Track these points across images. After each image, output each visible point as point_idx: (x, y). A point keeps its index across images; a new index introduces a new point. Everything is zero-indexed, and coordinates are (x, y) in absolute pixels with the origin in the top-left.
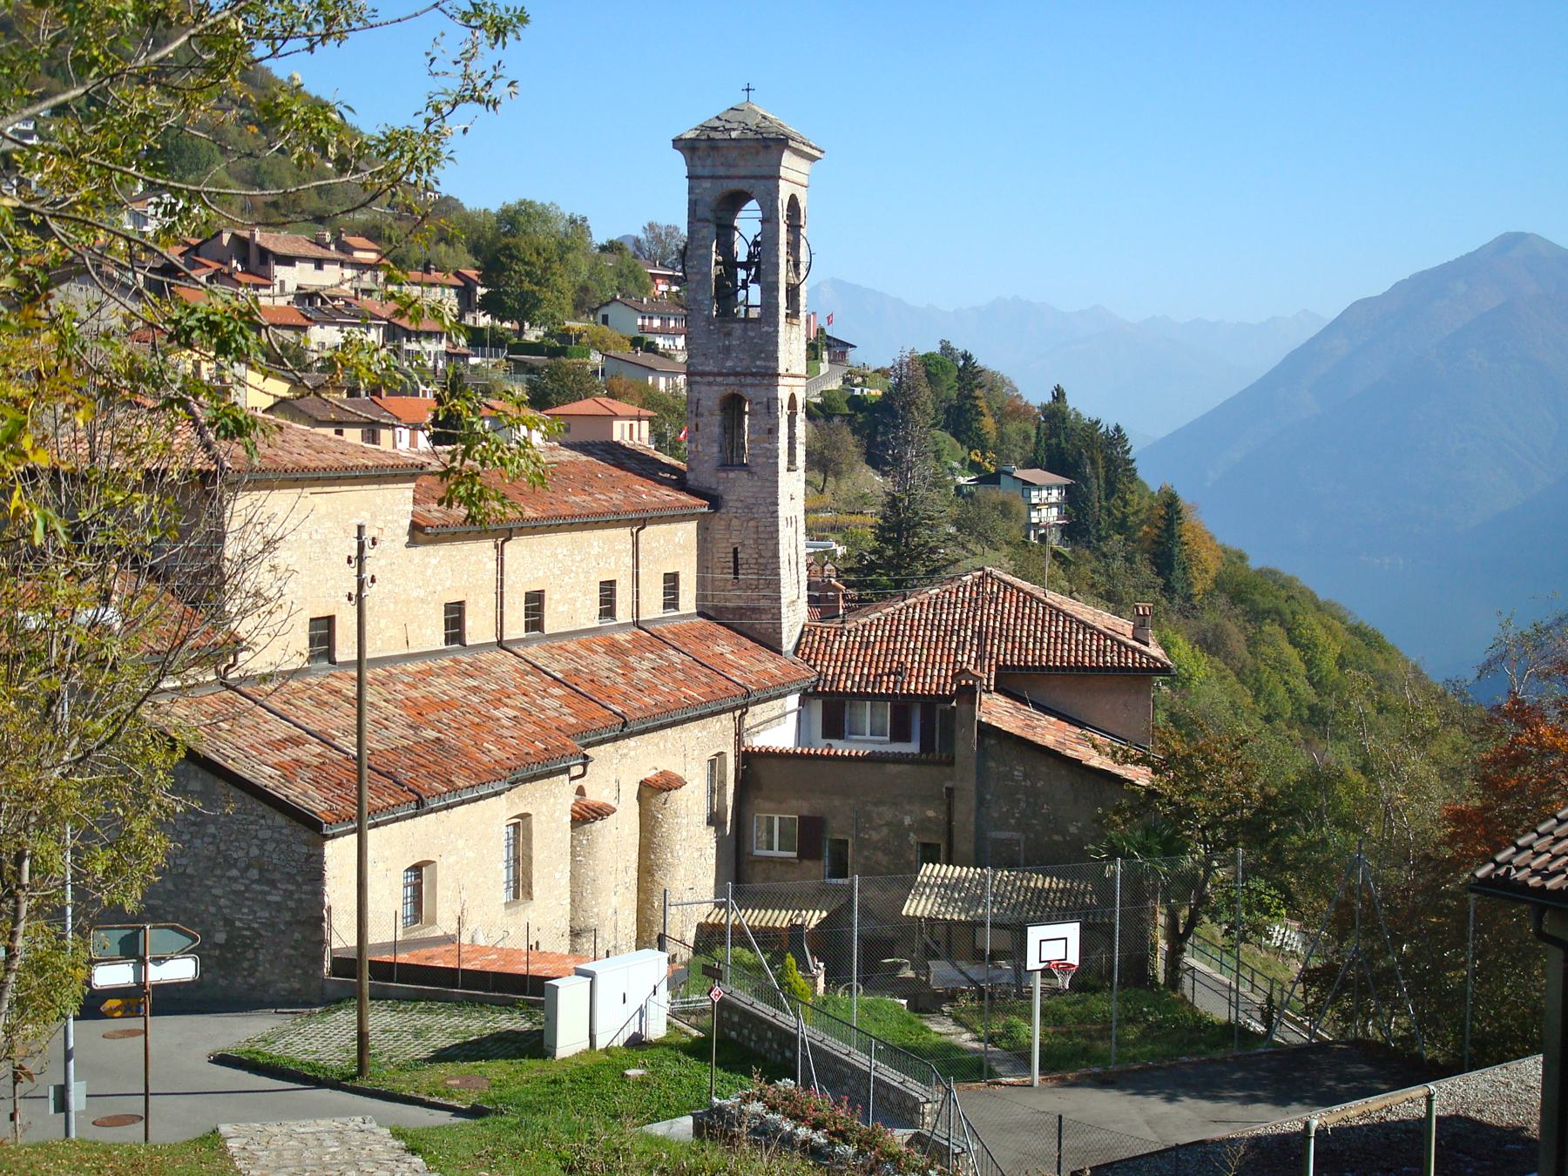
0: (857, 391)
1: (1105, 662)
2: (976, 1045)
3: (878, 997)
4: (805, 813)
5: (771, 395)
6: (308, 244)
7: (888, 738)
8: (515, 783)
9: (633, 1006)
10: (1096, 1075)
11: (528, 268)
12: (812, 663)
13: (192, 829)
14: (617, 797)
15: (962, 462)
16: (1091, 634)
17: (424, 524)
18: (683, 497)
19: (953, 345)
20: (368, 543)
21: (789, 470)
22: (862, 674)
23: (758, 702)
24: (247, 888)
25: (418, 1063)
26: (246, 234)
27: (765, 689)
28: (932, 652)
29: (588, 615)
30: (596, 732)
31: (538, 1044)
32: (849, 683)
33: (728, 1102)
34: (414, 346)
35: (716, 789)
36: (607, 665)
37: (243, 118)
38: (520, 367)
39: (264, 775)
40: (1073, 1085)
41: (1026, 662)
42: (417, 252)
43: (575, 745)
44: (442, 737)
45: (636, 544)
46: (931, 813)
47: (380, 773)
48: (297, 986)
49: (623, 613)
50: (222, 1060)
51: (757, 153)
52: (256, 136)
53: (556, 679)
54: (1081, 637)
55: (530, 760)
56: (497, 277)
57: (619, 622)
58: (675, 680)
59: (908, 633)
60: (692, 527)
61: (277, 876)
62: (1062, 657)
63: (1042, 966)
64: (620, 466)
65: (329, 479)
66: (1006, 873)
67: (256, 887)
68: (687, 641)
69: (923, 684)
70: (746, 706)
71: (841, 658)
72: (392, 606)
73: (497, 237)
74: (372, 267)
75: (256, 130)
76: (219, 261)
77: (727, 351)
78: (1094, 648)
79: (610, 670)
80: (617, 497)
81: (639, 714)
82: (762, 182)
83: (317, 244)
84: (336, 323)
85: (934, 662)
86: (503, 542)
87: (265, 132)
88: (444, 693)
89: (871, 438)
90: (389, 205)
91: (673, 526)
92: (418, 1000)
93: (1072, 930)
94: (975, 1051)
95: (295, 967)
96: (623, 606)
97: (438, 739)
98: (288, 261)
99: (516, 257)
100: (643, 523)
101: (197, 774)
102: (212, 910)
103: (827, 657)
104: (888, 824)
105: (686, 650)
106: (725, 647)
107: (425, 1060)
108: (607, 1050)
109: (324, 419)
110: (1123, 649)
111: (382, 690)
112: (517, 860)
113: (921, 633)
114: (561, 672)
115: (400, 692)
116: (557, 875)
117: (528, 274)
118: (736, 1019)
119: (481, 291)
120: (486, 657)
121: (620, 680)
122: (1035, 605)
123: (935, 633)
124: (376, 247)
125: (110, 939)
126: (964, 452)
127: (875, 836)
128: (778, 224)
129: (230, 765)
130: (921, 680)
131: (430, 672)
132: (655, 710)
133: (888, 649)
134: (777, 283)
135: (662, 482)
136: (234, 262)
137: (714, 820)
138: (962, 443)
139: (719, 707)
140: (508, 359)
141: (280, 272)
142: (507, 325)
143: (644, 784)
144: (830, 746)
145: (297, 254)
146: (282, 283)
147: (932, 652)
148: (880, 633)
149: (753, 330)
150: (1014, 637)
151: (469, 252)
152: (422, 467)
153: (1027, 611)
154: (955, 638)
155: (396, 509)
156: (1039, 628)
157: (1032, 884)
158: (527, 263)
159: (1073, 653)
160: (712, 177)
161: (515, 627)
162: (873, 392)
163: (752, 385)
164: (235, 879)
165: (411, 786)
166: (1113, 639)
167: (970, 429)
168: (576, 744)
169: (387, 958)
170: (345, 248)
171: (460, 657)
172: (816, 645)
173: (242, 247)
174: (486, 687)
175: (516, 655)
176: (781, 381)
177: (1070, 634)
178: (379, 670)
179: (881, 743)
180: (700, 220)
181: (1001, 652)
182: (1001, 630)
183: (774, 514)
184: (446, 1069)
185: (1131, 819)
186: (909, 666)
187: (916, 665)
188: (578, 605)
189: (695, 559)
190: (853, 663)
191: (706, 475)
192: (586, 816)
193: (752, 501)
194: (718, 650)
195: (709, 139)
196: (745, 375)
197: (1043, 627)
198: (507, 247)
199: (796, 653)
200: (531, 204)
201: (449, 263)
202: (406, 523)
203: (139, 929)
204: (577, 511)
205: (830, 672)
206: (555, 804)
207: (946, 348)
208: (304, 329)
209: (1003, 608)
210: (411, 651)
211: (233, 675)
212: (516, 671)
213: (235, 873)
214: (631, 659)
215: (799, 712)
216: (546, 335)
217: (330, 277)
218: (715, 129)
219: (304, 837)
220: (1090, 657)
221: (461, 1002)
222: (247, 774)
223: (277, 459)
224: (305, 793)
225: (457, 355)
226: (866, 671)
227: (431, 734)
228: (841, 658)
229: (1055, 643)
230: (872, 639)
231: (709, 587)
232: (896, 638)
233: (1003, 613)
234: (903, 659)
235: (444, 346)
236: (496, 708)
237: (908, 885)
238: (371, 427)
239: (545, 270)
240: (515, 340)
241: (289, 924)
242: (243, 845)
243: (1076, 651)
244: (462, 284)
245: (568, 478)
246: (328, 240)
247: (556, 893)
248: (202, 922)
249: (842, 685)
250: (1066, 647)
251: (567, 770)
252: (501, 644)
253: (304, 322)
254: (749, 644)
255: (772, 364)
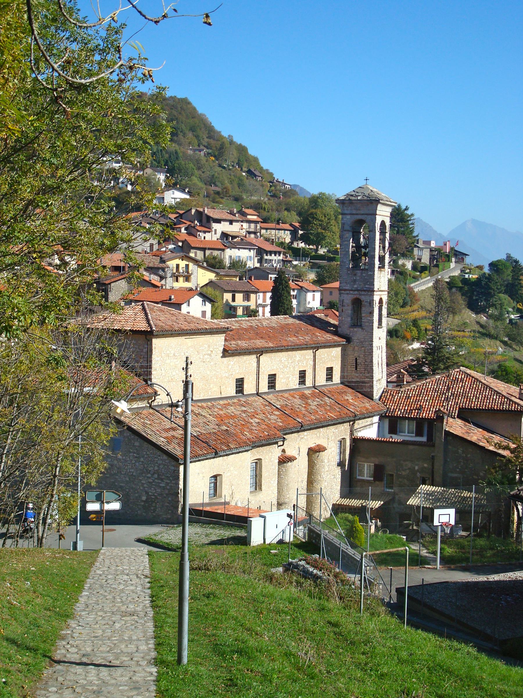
0: (467, 276)
1: (503, 408)
2: (427, 555)
3: (394, 535)
4: (377, 463)
5: (371, 299)
6: (227, 214)
7: (414, 435)
8: (253, 447)
9: (280, 529)
10: (463, 566)
11: (321, 223)
12: (385, 404)
13: (136, 459)
14: (299, 454)
15: (513, 308)
16: (499, 396)
17: (228, 349)
18: (335, 338)
19: (512, 255)
20: (189, 363)
21: (378, 328)
22: (405, 409)
23: (360, 419)
24: (154, 481)
25: (204, 545)
26: (201, 210)
27: (363, 414)
28: (434, 401)
29: (294, 383)
30: (290, 429)
31: (245, 541)
32: (399, 412)
33: (294, 561)
34: (268, 257)
35: (342, 452)
36: (299, 403)
37: (208, 154)
38: (313, 266)
39: (161, 441)
40: (453, 570)
41: (471, 406)
42: (275, 215)
43: (281, 434)
44: (228, 429)
45: (315, 356)
46: (426, 465)
47: (203, 442)
48: (169, 517)
49: (309, 382)
50: (139, 540)
51: (368, 205)
52: (213, 161)
53: (277, 408)
54: (495, 397)
55: (261, 439)
56: (307, 227)
57: (307, 386)
58: (326, 410)
59: (425, 393)
60: (339, 349)
61: (163, 477)
62: (486, 405)
63: (440, 524)
64: (312, 325)
65: (191, 333)
66: (453, 490)
67: (156, 481)
68: (334, 394)
69: (429, 414)
70: (354, 421)
71: (397, 402)
72: (215, 380)
73: (308, 210)
74: (256, 222)
75: (213, 159)
76: (190, 221)
77: (355, 281)
78: (500, 402)
79: (300, 405)
80: (307, 338)
81: (308, 423)
82: (370, 216)
83: (231, 214)
84: (236, 248)
85: (434, 405)
86: (260, 356)
87: (217, 160)
88: (233, 412)
89: (470, 298)
90: (269, 191)
91: (331, 349)
92: (210, 524)
93: (452, 512)
94: (426, 557)
95: (169, 510)
96: (309, 380)
97: (227, 430)
98: (218, 221)
99: (316, 218)
100: (317, 348)
101: (137, 439)
102: (141, 488)
103: (392, 402)
104: (409, 469)
105: (333, 398)
106: (350, 397)
107: (206, 544)
108: (270, 544)
109: (228, 289)
110: (511, 403)
111: (209, 411)
112: (256, 476)
113: (430, 393)
114: (280, 405)
115: (215, 412)
116: (272, 482)
117: (320, 225)
118: (315, 536)
119: (301, 232)
120: (251, 399)
121: (303, 409)
122: (478, 383)
123: (436, 394)
124: (257, 214)
125: (91, 495)
126: (514, 304)
127: (404, 473)
128: (375, 232)
129: (149, 437)
130: (428, 412)
131: (229, 404)
132: (315, 421)
133: (416, 399)
134: (374, 255)
135: (328, 332)
136: (196, 222)
137: (341, 464)
138: (514, 300)
139: (343, 421)
140: (310, 262)
141: (215, 226)
142: (311, 247)
143: (310, 449)
144: (391, 437)
145: (222, 218)
146: (216, 230)
147: (434, 401)
148: (414, 393)
149: (364, 273)
150: (468, 396)
151: (297, 215)
152: (228, 328)
153: (475, 386)
154: (444, 396)
155: (218, 344)
156: (478, 393)
157: (462, 495)
158: (320, 221)
159: (491, 404)
160: (350, 214)
161: (264, 387)
162: (474, 276)
163: (364, 295)
164: (149, 478)
165: (214, 447)
166: (508, 398)
167: (517, 294)
168: (280, 433)
169: (201, 508)
170: (244, 214)
171: (241, 399)
172: (388, 397)
173: (200, 215)
174: (249, 411)
175: (263, 398)
176: (375, 293)
177: (491, 396)
178: (209, 403)
179: (411, 437)
180: (345, 231)
181: (463, 403)
182: (463, 393)
183: (371, 345)
184: (210, 547)
185: (499, 471)
186: (424, 406)
187: (427, 406)
188: (290, 379)
189: (340, 362)
190: (402, 405)
191: (345, 329)
192: (285, 460)
193: (362, 340)
194: (346, 398)
195: (349, 200)
196: (362, 291)
197: (480, 393)
198: (312, 214)
199: (380, 400)
200: (324, 194)
201: (288, 220)
202: (221, 349)
203: (102, 492)
204: (290, 344)
205: (392, 408)
206: (271, 456)
207: (509, 257)
208: (223, 250)
209: (465, 384)
210: (222, 396)
211: (155, 403)
212: (262, 405)
213: (149, 475)
214: (309, 401)
215: (379, 423)
216: (327, 251)
217: (234, 229)
218: (352, 195)
219: (173, 463)
220: (497, 406)
221: (224, 525)
222: (154, 440)
223: (173, 326)
224: (174, 448)
225: (287, 261)
226: (406, 408)
227: (224, 428)
228: (397, 402)
229: (484, 400)
230: (411, 395)
231: (346, 371)
232: (420, 395)
233: (464, 386)
234: (422, 404)
235: (281, 257)
236: (252, 419)
237: (412, 491)
238: (247, 293)
239: (328, 223)
240: (314, 253)
241: (167, 494)
242: (152, 465)
243: (492, 403)
244: (293, 229)
245: (289, 331)
246: (235, 212)
247: (272, 489)
248: (138, 492)
249: (396, 413)
250: (488, 401)
251: (277, 443)
252: (258, 394)
253: (223, 247)
254: (360, 395)
255: (372, 287)
